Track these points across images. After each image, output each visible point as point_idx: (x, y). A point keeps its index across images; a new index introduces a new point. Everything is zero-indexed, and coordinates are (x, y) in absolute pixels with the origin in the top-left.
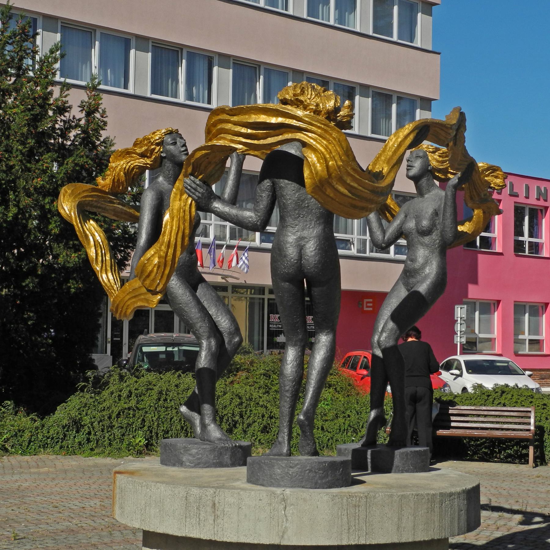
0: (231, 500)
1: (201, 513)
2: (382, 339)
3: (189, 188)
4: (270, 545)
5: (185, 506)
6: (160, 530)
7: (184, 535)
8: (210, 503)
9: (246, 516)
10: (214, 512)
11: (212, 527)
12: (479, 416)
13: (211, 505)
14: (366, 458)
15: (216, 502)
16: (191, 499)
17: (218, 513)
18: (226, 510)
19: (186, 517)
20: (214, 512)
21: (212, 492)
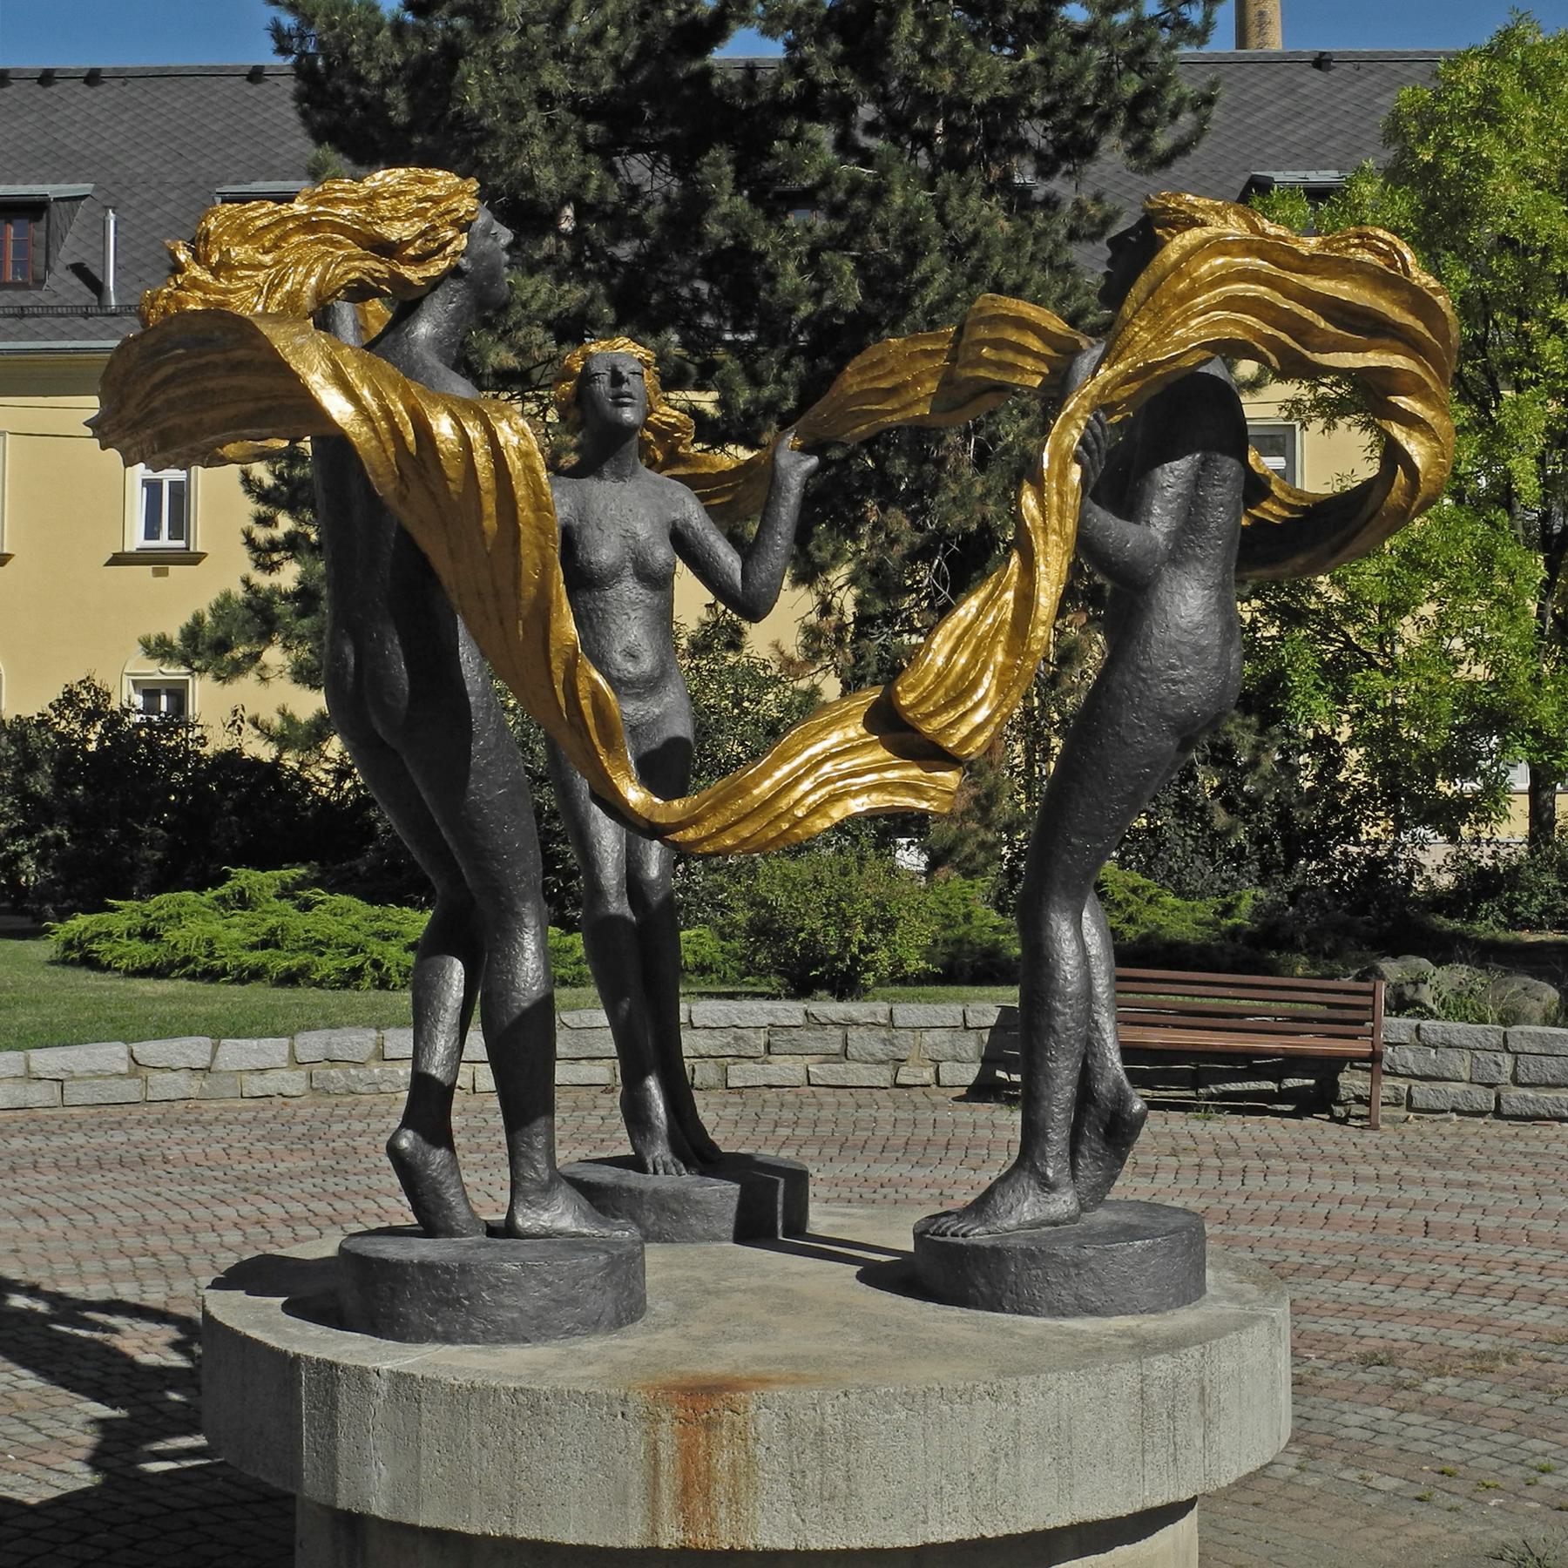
0: (1228, 1365)
7: (1138, 1508)
8: (1194, 1391)
13: (1196, 1395)
16: (1155, 1392)
19: (1144, 1451)
21: (1197, 1355)
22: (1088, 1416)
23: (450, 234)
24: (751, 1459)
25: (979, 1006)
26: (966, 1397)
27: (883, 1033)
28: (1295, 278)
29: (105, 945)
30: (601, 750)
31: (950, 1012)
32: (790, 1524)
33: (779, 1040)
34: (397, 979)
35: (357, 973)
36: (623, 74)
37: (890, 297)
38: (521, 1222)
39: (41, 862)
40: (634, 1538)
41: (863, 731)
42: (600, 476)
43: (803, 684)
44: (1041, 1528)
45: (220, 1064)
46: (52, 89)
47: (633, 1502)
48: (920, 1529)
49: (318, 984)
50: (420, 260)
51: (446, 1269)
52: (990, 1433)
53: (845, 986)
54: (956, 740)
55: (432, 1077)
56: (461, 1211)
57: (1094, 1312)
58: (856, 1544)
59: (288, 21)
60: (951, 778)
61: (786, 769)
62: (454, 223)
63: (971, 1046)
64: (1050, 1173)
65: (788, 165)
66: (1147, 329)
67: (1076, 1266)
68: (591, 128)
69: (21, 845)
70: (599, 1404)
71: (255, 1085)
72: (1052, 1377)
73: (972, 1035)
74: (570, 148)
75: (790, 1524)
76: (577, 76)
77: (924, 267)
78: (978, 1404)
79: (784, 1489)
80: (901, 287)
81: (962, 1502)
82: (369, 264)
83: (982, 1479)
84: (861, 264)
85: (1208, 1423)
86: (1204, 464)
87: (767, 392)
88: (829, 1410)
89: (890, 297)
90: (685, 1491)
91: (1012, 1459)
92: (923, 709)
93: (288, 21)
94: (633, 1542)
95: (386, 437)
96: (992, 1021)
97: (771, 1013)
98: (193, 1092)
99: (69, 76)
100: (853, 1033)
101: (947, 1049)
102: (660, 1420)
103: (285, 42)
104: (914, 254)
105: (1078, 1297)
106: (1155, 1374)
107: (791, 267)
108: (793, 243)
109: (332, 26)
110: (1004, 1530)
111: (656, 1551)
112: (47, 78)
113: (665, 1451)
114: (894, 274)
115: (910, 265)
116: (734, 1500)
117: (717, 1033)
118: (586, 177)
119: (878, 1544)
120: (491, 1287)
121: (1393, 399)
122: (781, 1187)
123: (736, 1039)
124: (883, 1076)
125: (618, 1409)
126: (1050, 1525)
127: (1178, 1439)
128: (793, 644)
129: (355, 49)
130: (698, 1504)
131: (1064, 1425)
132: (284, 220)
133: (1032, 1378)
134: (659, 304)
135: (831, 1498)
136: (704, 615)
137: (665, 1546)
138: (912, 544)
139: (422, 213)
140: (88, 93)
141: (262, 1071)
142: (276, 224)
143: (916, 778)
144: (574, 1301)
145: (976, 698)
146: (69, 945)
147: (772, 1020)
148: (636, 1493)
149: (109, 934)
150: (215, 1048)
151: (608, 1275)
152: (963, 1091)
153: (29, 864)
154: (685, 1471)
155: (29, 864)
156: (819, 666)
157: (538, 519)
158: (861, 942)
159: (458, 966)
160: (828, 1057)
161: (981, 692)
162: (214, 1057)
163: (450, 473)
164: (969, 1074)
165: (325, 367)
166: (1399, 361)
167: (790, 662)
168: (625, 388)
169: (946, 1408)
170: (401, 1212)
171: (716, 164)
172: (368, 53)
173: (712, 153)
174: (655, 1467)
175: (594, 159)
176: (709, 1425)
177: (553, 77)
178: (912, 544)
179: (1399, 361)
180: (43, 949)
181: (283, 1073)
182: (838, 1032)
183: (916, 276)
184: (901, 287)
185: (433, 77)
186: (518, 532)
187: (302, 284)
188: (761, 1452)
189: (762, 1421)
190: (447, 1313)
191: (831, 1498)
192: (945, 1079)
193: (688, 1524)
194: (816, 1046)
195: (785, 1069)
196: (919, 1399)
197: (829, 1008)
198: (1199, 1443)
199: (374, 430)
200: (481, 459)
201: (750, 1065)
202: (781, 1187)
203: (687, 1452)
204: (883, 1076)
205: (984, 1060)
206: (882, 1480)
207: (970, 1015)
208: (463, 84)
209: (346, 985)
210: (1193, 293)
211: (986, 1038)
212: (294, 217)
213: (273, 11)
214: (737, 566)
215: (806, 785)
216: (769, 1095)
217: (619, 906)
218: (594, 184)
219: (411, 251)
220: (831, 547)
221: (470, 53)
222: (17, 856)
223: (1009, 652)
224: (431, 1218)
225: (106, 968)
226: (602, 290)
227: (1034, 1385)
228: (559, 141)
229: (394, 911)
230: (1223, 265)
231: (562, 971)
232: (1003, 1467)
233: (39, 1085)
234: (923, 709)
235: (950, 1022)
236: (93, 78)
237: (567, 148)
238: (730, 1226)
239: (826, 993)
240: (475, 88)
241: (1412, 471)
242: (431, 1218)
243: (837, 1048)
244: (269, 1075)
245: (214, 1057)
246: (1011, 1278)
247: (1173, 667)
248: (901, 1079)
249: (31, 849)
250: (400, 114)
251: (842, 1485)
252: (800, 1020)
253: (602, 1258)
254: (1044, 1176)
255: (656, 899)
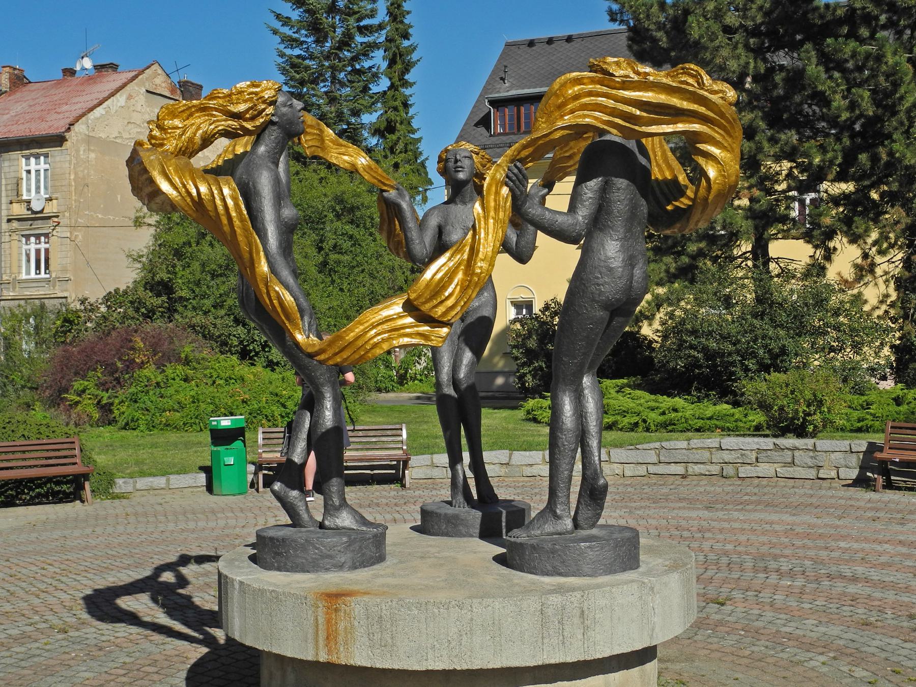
0: (603, 602)
1: (566, 627)
2: (462, 375)
3: (514, 178)
4: (633, 652)
5: (540, 623)
6: (497, 665)
7: (540, 663)
8: (577, 612)
9: (619, 619)
10: (583, 623)
11: (581, 643)
12: (13, 452)
13: (578, 614)
14: (501, 521)
15: (585, 608)
16: (550, 612)
17: (588, 623)
18: (597, 616)
19: (543, 638)
20: (583, 623)
21: (579, 596)
22: (510, 620)
23: (263, 107)
24: (352, 626)
25: (857, 442)
26: (446, 606)
27: (811, 454)
28: (614, 92)
29: (540, 412)
30: (286, 322)
31: (844, 444)
32: (368, 656)
33: (762, 456)
34: (653, 428)
35: (636, 424)
36: (767, 14)
37: (885, 108)
38: (327, 523)
39: (534, 377)
40: (310, 657)
41: (401, 310)
42: (456, 204)
43: (855, 291)
44: (485, 667)
45: (513, 462)
46: (552, 46)
47: (309, 641)
48: (424, 663)
49: (621, 430)
50: (253, 118)
51: (278, 540)
52: (458, 623)
53: (801, 432)
54: (439, 313)
55: (294, 462)
56: (305, 516)
57: (560, 574)
58: (396, 667)
59: (615, 7)
60: (444, 331)
61: (362, 327)
62: (264, 102)
63: (854, 461)
64: (558, 511)
65: (835, 50)
66: (545, 123)
67: (552, 553)
68: (752, 41)
69: (525, 370)
70: (297, 599)
71: (528, 471)
72: (490, 600)
73: (854, 455)
74: (740, 50)
75: (368, 656)
76: (745, 17)
77: (902, 90)
78: (452, 610)
79: (365, 639)
80: (890, 101)
81: (444, 653)
82: (230, 122)
83: (454, 643)
84: (874, 92)
85: (586, 629)
86: (606, 183)
87: (830, 155)
88: (384, 607)
89: (885, 108)
90: (327, 638)
91: (469, 635)
92: (421, 300)
93: (615, 7)
94: (310, 658)
95: (184, 194)
96: (864, 449)
97: (758, 443)
98: (502, 474)
99: (559, 39)
100: (797, 453)
101: (842, 462)
102: (318, 607)
103: (615, 17)
104: (896, 85)
105: (554, 567)
106: (549, 603)
107: (838, 97)
108: (838, 85)
109: (631, 7)
110: (465, 667)
111: (318, 662)
112: (550, 41)
113: (321, 620)
114: (888, 95)
115: (895, 91)
116: (346, 643)
117: (733, 452)
118: (748, 63)
119: (405, 668)
120: (293, 548)
121: (698, 145)
122: (504, 515)
123: (742, 455)
124: (812, 474)
125: (304, 601)
126: (490, 666)
127: (565, 634)
128: (849, 273)
129: (642, 16)
130: (332, 644)
131: (496, 622)
132: (190, 108)
133: (479, 600)
134: (787, 119)
135: (385, 646)
136: (808, 261)
137: (321, 660)
138: (907, 224)
139: (251, 100)
140: (568, 46)
141: (531, 465)
142: (187, 109)
143: (427, 331)
144: (331, 557)
145: (447, 294)
146: (528, 412)
147: (758, 447)
148: (310, 637)
149: (541, 408)
150: (511, 455)
151: (349, 545)
152: (851, 482)
153: (529, 378)
154: (328, 629)
155: (529, 378)
156: (862, 283)
157: (243, 225)
158: (804, 411)
159: (309, 414)
160: (786, 464)
161: (450, 290)
162: (510, 459)
163: (209, 208)
164: (854, 474)
165: (158, 167)
166: (696, 127)
167: (846, 281)
168: (459, 164)
169: (436, 611)
170: (285, 519)
171: (807, 51)
172: (648, 16)
173: (805, 46)
174: (317, 627)
175: (751, 55)
176: (336, 610)
177: (732, 19)
178: (907, 224)
179: (696, 127)
180: (520, 414)
181: (540, 466)
182: (790, 453)
183: (898, 95)
184: (890, 101)
185: (678, 25)
186: (235, 232)
187: (195, 134)
188: (356, 624)
189: (356, 610)
190: (278, 558)
191: (385, 646)
192: (842, 476)
193: (329, 652)
194: (779, 459)
195: (765, 469)
196: (423, 606)
197: (790, 441)
198: (580, 637)
199: (179, 192)
200: (218, 202)
201: (749, 467)
202: (504, 515)
203: (328, 621)
204: (812, 474)
205: (861, 468)
206: (406, 640)
207: (853, 446)
208: (690, 26)
209: (632, 430)
210: (564, 104)
211: (861, 457)
212: (193, 106)
213: (607, 4)
214: (515, 239)
215: (373, 332)
216: (756, 481)
217: (450, 391)
218: (752, 65)
219: (248, 116)
220: (863, 227)
221: (693, 12)
222: (524, 375)
223: (466, 273)
224: (296, 522)
225: (540, 422)
226: (760, 114)
227: (480, 603)
228: (735, 47)
229: (661, 398)
230: (579, 90)
231: (728, 424)
232: (464, 638)
233: (437, 469)
234: (421, 300)
235: (844, 449)
236: (569, 39)
237: (738, 51)
238: (478, 531)
239: (791, 435)
240: (696, 29)
241: (708, 179)
242: (296, 522)
243: (789, 460)
244: (534, 467)
245: (510, 459)
246: (527, 557)
247: (598, 278)
248: (821, 476)
249: (530, 372)
250: (664, 42)
251: (390, 641)
252: (772, 447)
253: (345, 539)
254: (555, 512)
255: (464, 386)
